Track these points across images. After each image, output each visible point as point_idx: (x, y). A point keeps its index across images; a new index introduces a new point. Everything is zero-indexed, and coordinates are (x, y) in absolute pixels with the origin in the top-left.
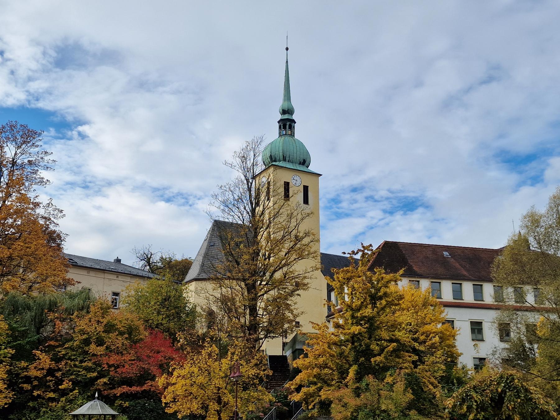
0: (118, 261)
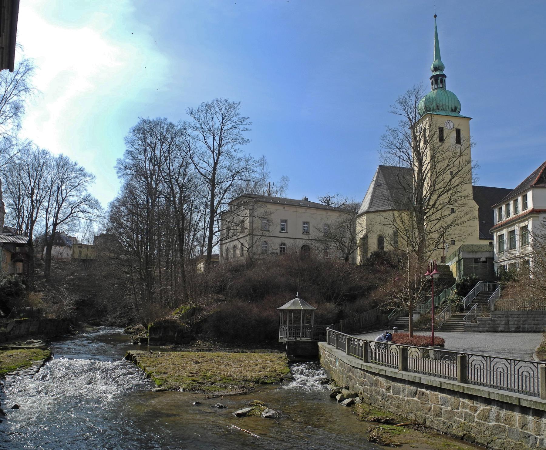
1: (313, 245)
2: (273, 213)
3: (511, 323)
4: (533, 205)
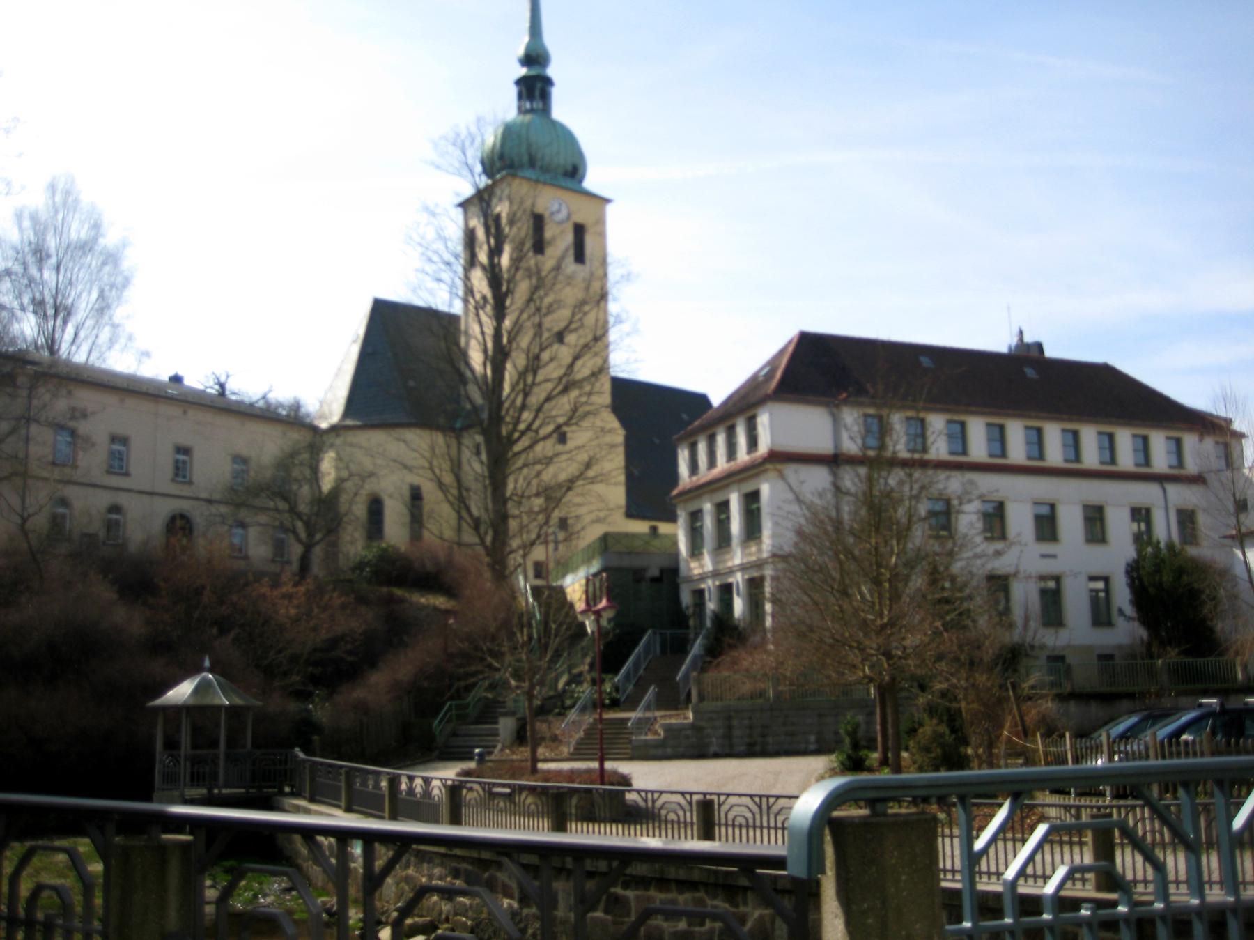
0: (176, 379)
1: (199, 514)
2: (93, 413)
3: (737, 732)
4: (772, 440)
